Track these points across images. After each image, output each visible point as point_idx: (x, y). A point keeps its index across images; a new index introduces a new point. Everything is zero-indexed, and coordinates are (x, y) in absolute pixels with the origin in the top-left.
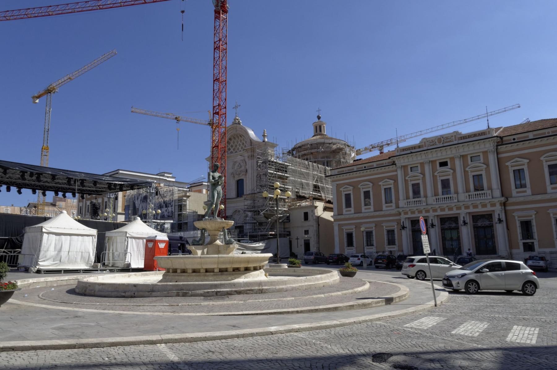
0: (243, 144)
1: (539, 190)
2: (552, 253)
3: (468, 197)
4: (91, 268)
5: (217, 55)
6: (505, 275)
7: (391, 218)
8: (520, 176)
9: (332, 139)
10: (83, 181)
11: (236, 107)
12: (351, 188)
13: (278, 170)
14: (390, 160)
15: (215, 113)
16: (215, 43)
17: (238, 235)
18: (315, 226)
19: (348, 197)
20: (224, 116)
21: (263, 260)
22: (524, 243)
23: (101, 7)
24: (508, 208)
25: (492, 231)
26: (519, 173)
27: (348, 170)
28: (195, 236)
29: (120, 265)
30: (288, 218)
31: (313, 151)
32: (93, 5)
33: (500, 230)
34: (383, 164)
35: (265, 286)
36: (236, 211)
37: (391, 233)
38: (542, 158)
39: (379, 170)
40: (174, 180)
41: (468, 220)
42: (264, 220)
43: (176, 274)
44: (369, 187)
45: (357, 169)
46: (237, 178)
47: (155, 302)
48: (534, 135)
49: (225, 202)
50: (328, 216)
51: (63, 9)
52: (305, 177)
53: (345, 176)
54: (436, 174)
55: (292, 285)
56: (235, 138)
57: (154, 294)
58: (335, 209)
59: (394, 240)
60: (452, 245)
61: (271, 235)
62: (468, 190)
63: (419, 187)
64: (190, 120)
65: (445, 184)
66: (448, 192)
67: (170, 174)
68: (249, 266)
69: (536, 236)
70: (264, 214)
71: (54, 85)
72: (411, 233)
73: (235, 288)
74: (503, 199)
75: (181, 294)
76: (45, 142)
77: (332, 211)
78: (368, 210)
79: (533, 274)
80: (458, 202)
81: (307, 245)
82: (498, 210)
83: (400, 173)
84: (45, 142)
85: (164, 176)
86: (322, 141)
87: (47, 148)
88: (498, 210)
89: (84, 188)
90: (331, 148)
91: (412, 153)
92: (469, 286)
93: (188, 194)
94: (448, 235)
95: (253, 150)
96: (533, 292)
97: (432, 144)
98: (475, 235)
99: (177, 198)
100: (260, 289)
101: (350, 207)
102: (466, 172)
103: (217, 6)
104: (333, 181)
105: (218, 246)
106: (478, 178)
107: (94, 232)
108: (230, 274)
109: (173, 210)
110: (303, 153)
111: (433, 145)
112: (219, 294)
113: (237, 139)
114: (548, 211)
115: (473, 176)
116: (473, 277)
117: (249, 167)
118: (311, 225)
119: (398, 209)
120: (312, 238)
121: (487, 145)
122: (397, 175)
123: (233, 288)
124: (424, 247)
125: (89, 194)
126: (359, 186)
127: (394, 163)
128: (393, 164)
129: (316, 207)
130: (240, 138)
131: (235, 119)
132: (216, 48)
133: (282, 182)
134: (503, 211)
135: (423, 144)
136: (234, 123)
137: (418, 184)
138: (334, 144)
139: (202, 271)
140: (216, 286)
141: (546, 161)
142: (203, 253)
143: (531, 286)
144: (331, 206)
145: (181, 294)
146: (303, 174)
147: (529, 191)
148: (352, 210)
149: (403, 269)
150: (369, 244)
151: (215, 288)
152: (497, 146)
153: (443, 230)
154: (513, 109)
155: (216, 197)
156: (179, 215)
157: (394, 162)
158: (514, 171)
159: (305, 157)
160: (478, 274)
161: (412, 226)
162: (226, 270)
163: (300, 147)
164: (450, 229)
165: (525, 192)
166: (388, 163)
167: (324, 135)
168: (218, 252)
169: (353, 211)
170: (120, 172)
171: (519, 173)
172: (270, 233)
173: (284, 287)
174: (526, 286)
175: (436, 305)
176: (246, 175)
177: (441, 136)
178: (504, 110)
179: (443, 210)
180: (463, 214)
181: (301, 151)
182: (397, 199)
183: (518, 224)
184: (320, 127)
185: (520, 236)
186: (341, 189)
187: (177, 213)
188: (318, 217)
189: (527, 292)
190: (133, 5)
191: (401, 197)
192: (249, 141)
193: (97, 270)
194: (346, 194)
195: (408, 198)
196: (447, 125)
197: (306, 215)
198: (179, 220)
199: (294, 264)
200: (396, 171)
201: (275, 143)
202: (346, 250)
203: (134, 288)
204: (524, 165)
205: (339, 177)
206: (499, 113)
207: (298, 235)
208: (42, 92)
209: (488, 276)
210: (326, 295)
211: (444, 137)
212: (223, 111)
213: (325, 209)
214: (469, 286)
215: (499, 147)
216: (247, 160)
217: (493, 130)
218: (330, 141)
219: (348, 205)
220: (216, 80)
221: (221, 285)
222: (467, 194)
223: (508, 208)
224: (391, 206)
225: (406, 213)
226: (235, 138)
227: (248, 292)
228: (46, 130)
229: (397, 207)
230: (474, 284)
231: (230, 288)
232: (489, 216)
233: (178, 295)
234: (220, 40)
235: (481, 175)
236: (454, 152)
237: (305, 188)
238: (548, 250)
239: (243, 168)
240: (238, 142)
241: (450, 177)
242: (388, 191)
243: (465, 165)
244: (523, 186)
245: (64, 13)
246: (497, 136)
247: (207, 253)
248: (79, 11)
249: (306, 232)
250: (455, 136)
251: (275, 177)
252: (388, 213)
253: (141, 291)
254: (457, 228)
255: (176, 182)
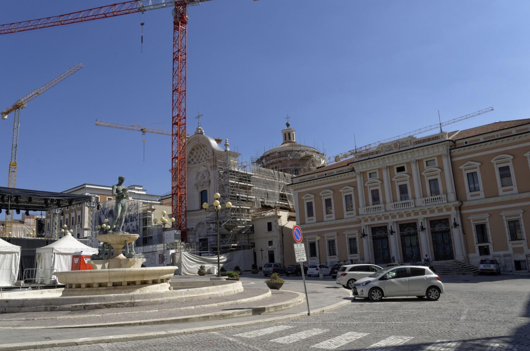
0: (206, 154)
1: (491, 193)
2: (505, 256)
3: (424, 202)
4: (13, 286)
5: (176, 66)
6: (409, 281)
7: (352, 226)
8: (473, 180)
9: (300, 146)
10: (17, 197)
11: (198, 117)
12: (313, 196)
13: (241, 180)
14: (349, 167)
15: (174, 124)
16: (174, 53)
17: (200, 248)
18: (278, 236)
19: (310, 205)
20: (183, 126)
21: (169, 272)
22: (479, 247)
23: (62, 22)
24: (464, 212)
25: (449, 236)
26: (472, 176)
27: (310, 178)
28: (154, 250)
29: (48, 282)
30: (252, 228)
31: (282, 159)
32: (55, 21)
33: (456, 234)
34: (343, 170)
35: (138, 299)
36: (200, 223)
37: (352, 241)
38: (492, 161)
39: (340, 177)
40: (144, 193)
41: (426, 225)
42: (225, 231)
43: (71, 289)
44: (330, 195)
45: (318, 176)
46: (201, 189)
47: (12, 317)
48: (484, 138)
49: (186, 214)
50: (291, 225)
51: (26, 25)
52: (270, 187)
53: (306, 184)
54: (393, 179)
55: (169, 298)
56: (197, 148)
57: (23, 309)
58: (298, 218)
59: (356, 248)
60: (412, 251)
61: (233, 247)
62: (424, 196)
63: (378, 194)
64: (151, 130)
65: (403, 190)
66: (406, 198)
67: (141, 186)
68: (144, 280)
69: (490, 239)
70: (225, 225)
71: (22, 100)
72: (372, 240)
73: (105, 301)
74: (457, 203)
75: (49, 309)
76: (13, 159)
77: (295, 220)
78: (330, 219)
79: (438, 279)
80: (416, 207)
81: (271, 256)
82: (453, 215)
83: (359, 180)
84: (13, 159)
85: (134, 189)
86: (291, 148)
87: (15, 165)
88: (453, 215)
89: (20, 204)
90: (300, 155)
91: (369, 159)
92: (373, 293)
93: (153, 207)
94: (408, 241)
95: (215, 160)
96: (437, 297)
97: (388, 149)
98: (433, 241)
99: (141, 211)
100: (131, 303)
101: (312, 216)
102: (422, 177)
103: (175, 17)
104: (295, 190)
105: (120, 260)
106: (434, 182)
107: (17, 249)
108: (123, 289)
109: (138, 224)
110: (271, 161)
111: (390, 150)
112: (87, 308)
113: (200, 149)
114: (501, 214)
115: (430, 181)
116: (376, 284)
117: (212, 178)
118: (275, 236)
119: (358, 217)
120: (276, 248)
121: (441, 149)
122: (356, 182)
123: (103, 302)
124: (296, 255)
125: (34, 210)
126: (320, 194)
127: (353, 170)
128: (351, 171)
129: (279, 217)
130: (203, 148)
131: (198, 129)
132: (175, 59)
133: (246, 192)
134: (459, 215)
135: (380, 149)
136: (197, 133)
137: (377, 190)
138: (302, 152)
139: (95, 285)
140: (85, 300)
141: (497, 164)
142: (103, 267)
143: (435, 291)
144: (293, 214)
145: (49, 309)
146: (268, 183)
147: (482, 194)
148: (314, 218)
149: (338, 279)
150: (332, 254)
151: (84, 303)
152: (450, 150)
153: (402, 237)
154: (486, 112)
155: (120, 211)
156: (144, 229)
157: (353, 168)
158: (467, 174)
159: (274, 166)
160: (382, 281)
161: (373, 234)
162: (134, 283)
163: (268, 155)
164: (410, 235)
165: (479, 195)
166: (348, 169)
167: (294, 142)
168: (120, 266)
169: (315, 220)
170: (87, 186)
171: (472, 176)
172: (232, 245)
173: (160, 299)
174: (430, 291)
175: (309, 314)
176: (209, 186)
177: (396, 141)
178: (478, 113)
179: (401, 216)
180: (421, 219)
181: (268, 161)
182: (358, 206)
183: (473, 228)
184: (289, 134)
185: (475, 240)
186: (303, 198)
187: (141, 227)
188: (282, 227)
189: (431, 297)
190: (94, 19)
191: (361, 204)
192: (211, 151)
193: (19, 288)
194: (307, 203)
195: (367, 205)
196: (424, 130)
197: (270, 225)
198: (144, 234)
199: (233, 276)
200: (355, 177)
201: (236, 151)
202: (328, 259)
203: (6, 304)
204: (477, 168)
205: (300, 186)
206: (473, 116)
207: (262, 245)
208: (10, 108)
209: (393, 283)
210: (197, 306)
211: (400, 141)
212: (183, 121)
213: (290, 218)
214: (373, 293)
215: (452, 151)
216: (210, 171)
217: (446, 134)
218: (299, 149)
219: (310, 214)
220: (175, 90)
221: (90, 298)
222: (424, 199)
223: (464, 212)
224: (352, 214)
225: (366, 220)
226: (197, 148)
227: (119, 305)
228: (14, 146)
229: (358, 214)
230: (378, 291)
231: (100, 302)
232: (445, 221)
233: (46, 310)
234: (179, 51)
235: (437, 179)
236: (410, 156)
237: (271, 198)
238: (501, 253)
239: (206, 179)
240: (201, 152)
241: (408, 183)
242: (348, 198)
243: (421, 170)
244: (476, 189)
245: (46, 27)
246: (449, 140)
247: (109, 268)
248: (41, 28)
249: (270, 243)
250: (410, 141)
251: (237, 187)
252: (349, 220)
253: (13, 307)
254: (416, 234)
255: (147, 195)
